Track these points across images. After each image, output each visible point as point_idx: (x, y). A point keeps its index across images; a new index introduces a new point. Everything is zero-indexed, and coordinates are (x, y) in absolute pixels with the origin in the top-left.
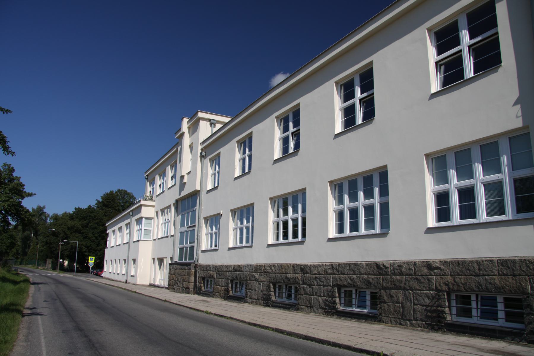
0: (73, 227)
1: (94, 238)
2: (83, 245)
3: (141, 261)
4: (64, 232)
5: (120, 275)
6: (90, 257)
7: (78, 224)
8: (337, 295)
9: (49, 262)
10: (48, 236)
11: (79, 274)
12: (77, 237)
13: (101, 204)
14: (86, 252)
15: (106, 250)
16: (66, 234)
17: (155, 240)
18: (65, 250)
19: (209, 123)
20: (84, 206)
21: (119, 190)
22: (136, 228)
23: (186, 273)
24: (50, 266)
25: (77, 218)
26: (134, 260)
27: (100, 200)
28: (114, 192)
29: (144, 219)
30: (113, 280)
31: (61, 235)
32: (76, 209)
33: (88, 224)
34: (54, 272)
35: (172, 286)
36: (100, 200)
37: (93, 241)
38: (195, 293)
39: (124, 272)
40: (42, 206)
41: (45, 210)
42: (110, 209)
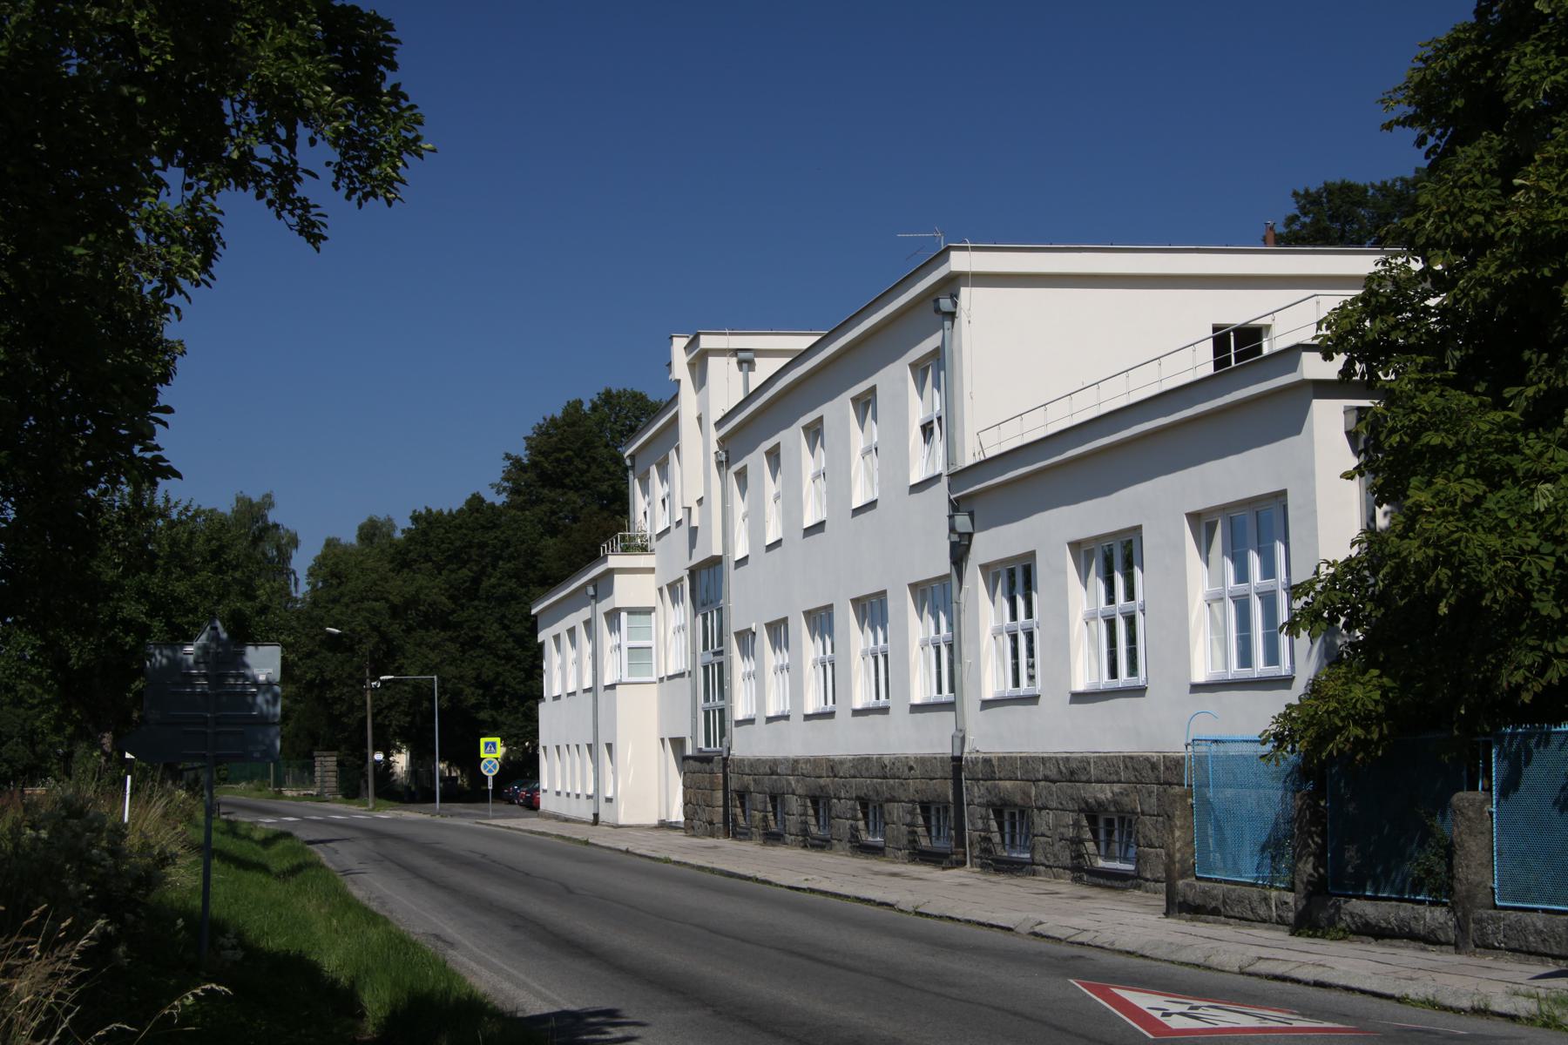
0: (412, 602)
1: (510, 644)
2: (461, 678)
3: (625, 751)
4: (376, 628)
5: (583, 797)
6: (483, 741)
7: (431, 587)
8: (1089, 835)
9: (326, 765)
10: (310, 655)
11: (458, 807)
12: (434, 648)
13: (531, 476)
14: (478, 707)
15: (541, 706)
16: (384, 637)
17: (661, 680)
18: (390, 707)
19: (734, 360)
20: (450, 501)
21: (608, 393)
22: (608, 640)
23: (728, 789)
24: (332, 781)
25: (427, 558)
26: (609, 746)
27: (522, 452)
28: (587, 407)
29: (624, 615)
30: (567, 820)
31: (367, 646)
32: (416, 518)
33: (476, 581)
34: (353, 808)
35: (691, 825)
36: (522, 452)
37: (509, 658)
38: (727, 835)
39: (590, 791)
40: (256, 498)
41: (272, 517)
42: (572, 495)
